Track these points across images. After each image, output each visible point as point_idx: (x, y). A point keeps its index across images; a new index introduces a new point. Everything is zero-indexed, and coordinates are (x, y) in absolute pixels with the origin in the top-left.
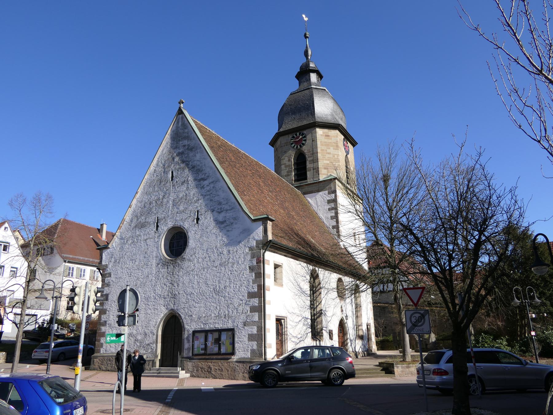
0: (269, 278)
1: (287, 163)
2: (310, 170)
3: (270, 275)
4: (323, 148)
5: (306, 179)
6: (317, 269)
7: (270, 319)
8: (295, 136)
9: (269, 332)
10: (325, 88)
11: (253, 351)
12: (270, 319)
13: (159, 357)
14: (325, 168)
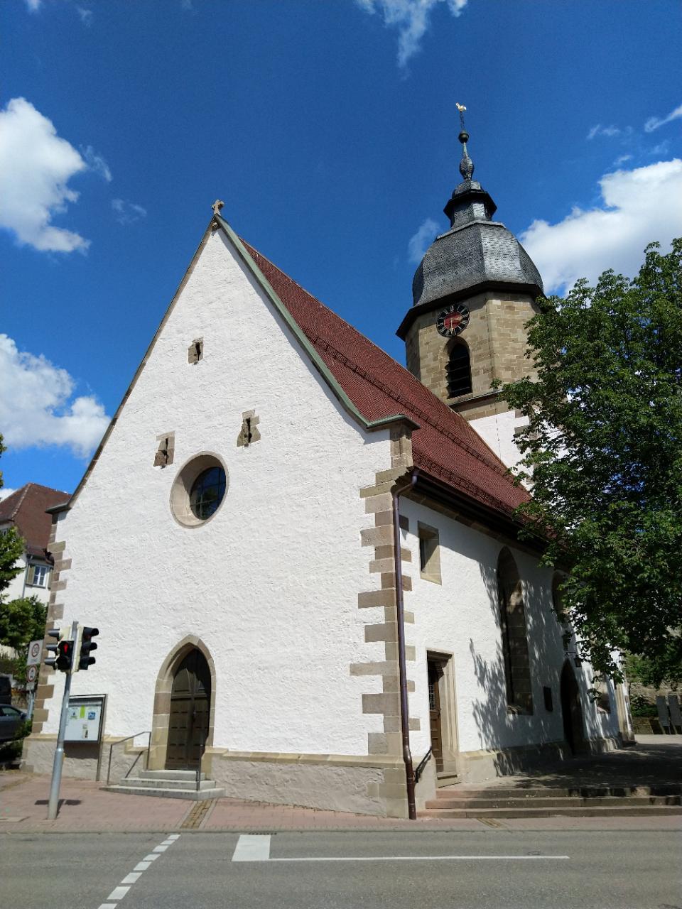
0: (410, 560)
1: (433, 364)
2: (477, 374)
3: (410, 553)
4: (503, 330)
5: (470, 391)
6: (510, 548)
7: (413, 659)
8: (447, 313)
9: (413, 690)
10: (501, 224)
11: (374, 740)
12: (413, 659)
13: (386, 559)
14: (508, 369)
